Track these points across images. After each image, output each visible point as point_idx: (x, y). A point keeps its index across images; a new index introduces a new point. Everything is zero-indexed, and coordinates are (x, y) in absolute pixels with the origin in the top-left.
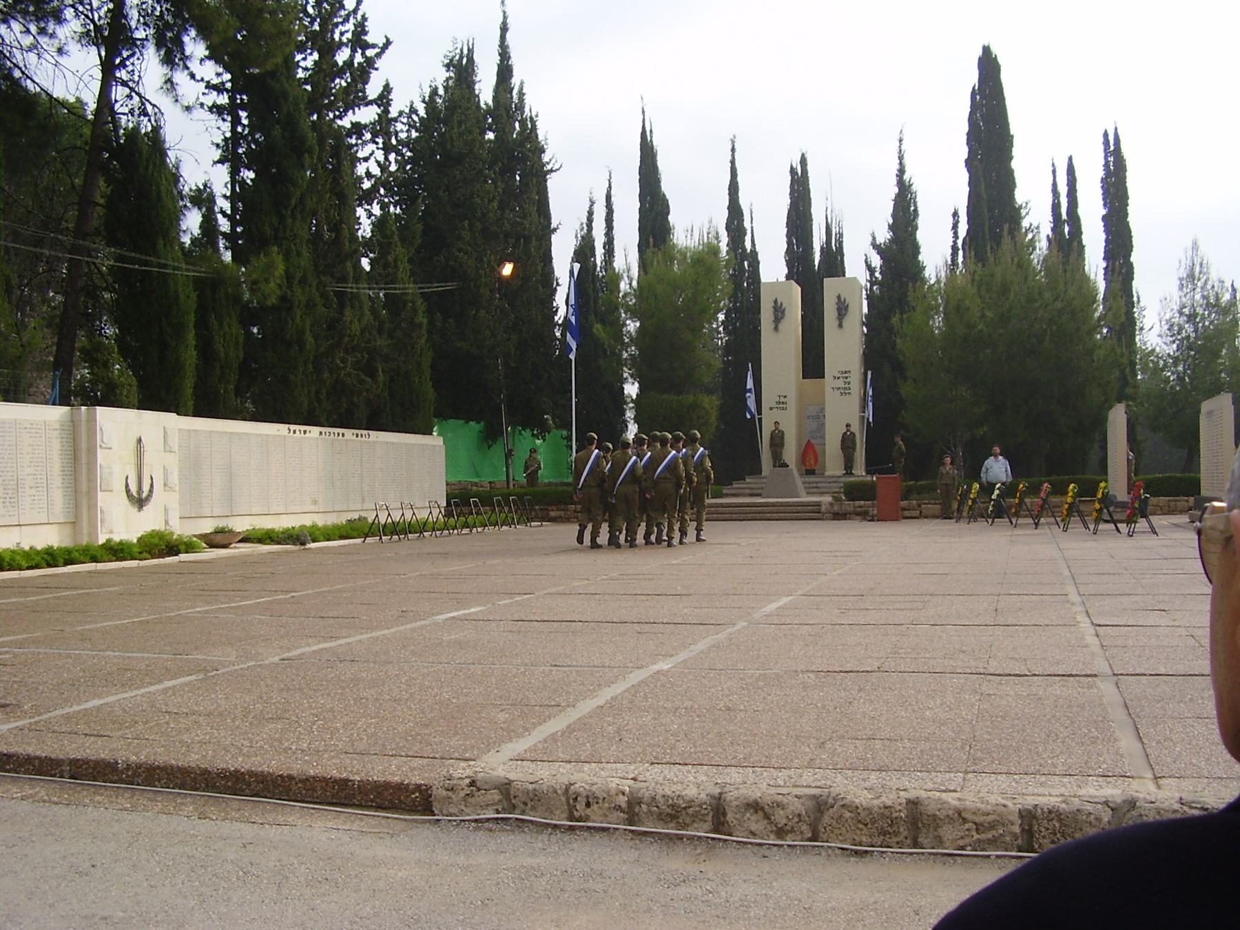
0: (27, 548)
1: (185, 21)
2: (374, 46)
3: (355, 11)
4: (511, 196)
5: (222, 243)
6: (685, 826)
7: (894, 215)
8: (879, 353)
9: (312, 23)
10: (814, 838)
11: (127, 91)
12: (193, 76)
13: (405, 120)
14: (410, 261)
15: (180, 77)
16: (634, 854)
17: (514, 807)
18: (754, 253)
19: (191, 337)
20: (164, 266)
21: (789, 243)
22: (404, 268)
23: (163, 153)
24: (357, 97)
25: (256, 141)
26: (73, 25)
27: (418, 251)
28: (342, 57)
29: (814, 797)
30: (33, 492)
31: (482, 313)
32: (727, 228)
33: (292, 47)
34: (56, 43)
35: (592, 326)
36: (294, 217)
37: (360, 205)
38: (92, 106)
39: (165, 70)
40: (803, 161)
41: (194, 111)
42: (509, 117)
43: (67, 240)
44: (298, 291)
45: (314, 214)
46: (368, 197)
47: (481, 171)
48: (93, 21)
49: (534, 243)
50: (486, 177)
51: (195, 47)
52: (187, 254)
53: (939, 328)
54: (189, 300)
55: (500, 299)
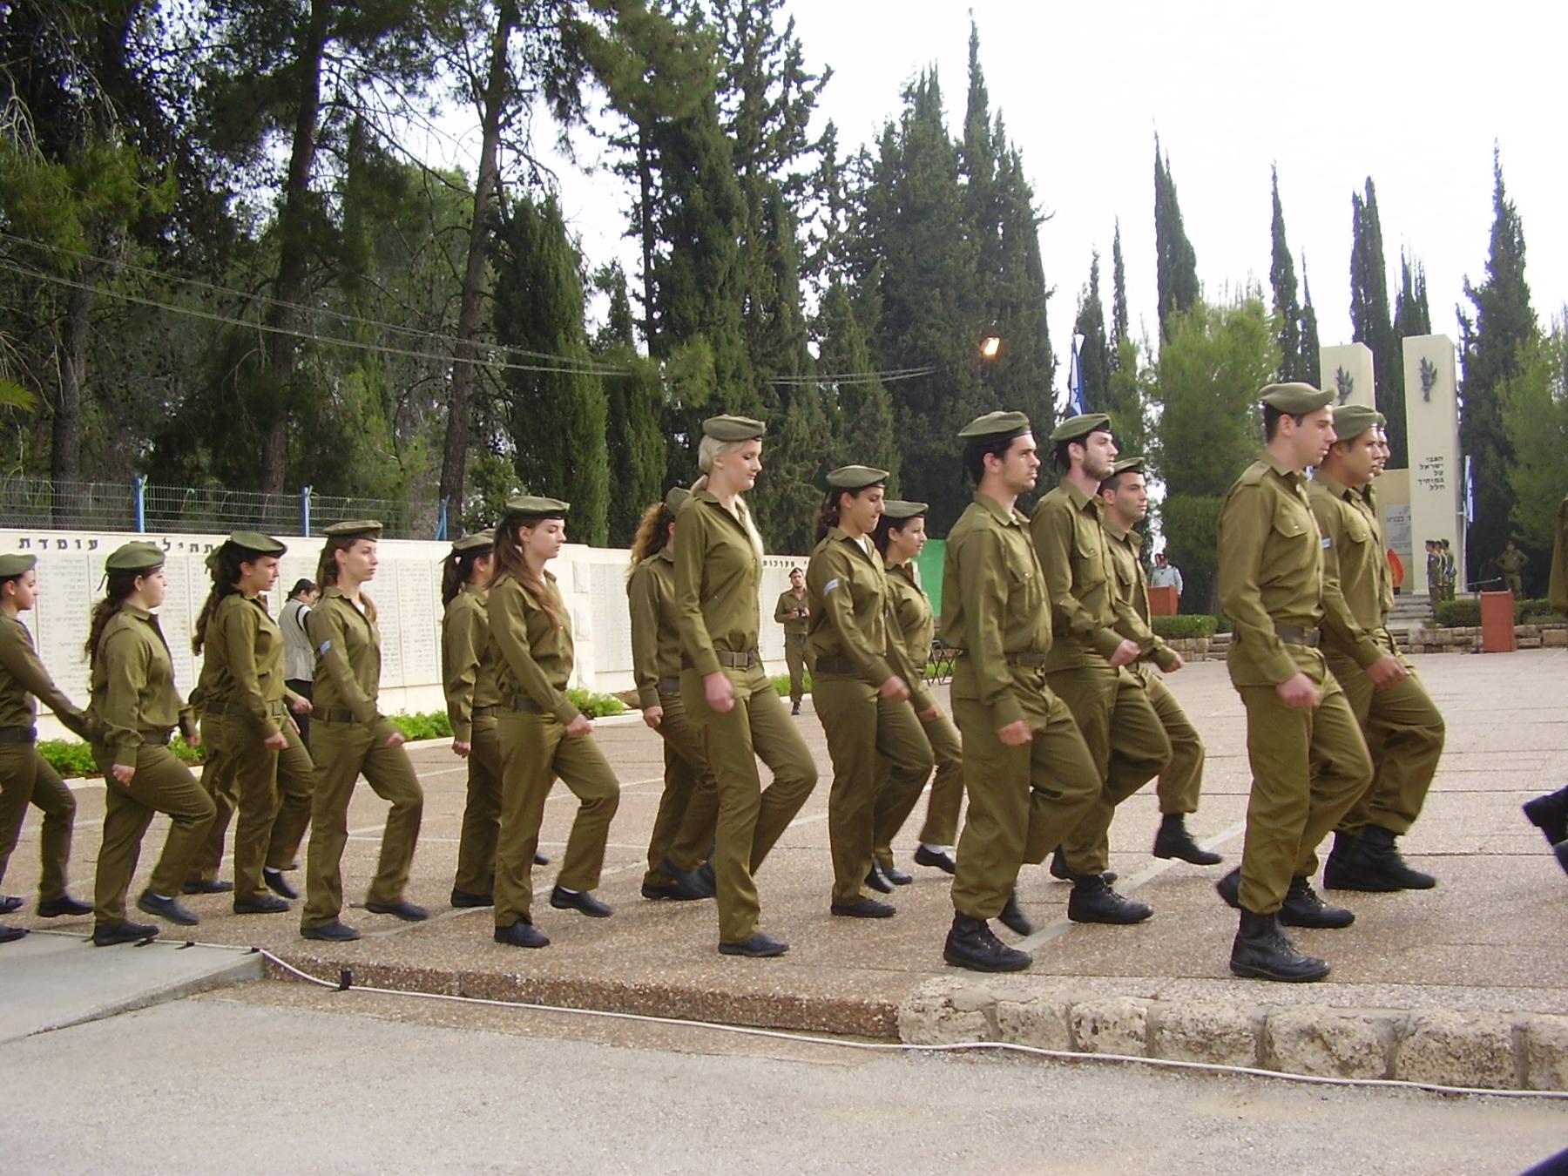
0: (413, 715)
1: (580, 64)
2: (811, 78)
3: (787, 36)
4: (991, 257)
5: (636, 333)
6: (1220, 1058)
7: (1493, 249)
8: (1480, 435)
9: (734, 55)
10: (1390, 1075)
11: (514, 154)
12: (592, 131)
13: (855, 168)
14: (869, 342)
15: (577, 132)
16: (1154, 1094)
17: (1001, 1033)
18: (1309, 310)
19: (603, 446)
20: (567, 365)
21: (1356, 294)
22: (861, 352)
23: (560, 228)
24: (795, 143)
25: (672, 206)
26: (447, 78)
28: (772, 94)
29: (1389, 1022)
30: (419, 646)
31: (962, 404)
32: (1273, 279)
33: (712, 86)
34: (427, 103)
36: (723, 298)
37: (804, 276)
38: (473, 177)
39: (559, 125)
40: (1370, 186)
41: (595, 173)
42: (985, 153)
43: (450, 340)
44: (731, 387)
45: (748, 291)
46: (813, 266)
47: (953, 225)
48: (470, 73)
49: (1024, 312)
50: (961, 232)
51: (593, 94)
52: (594, 349)
53: (1560, 396)
54: (597, 405)
55: (984, 385)
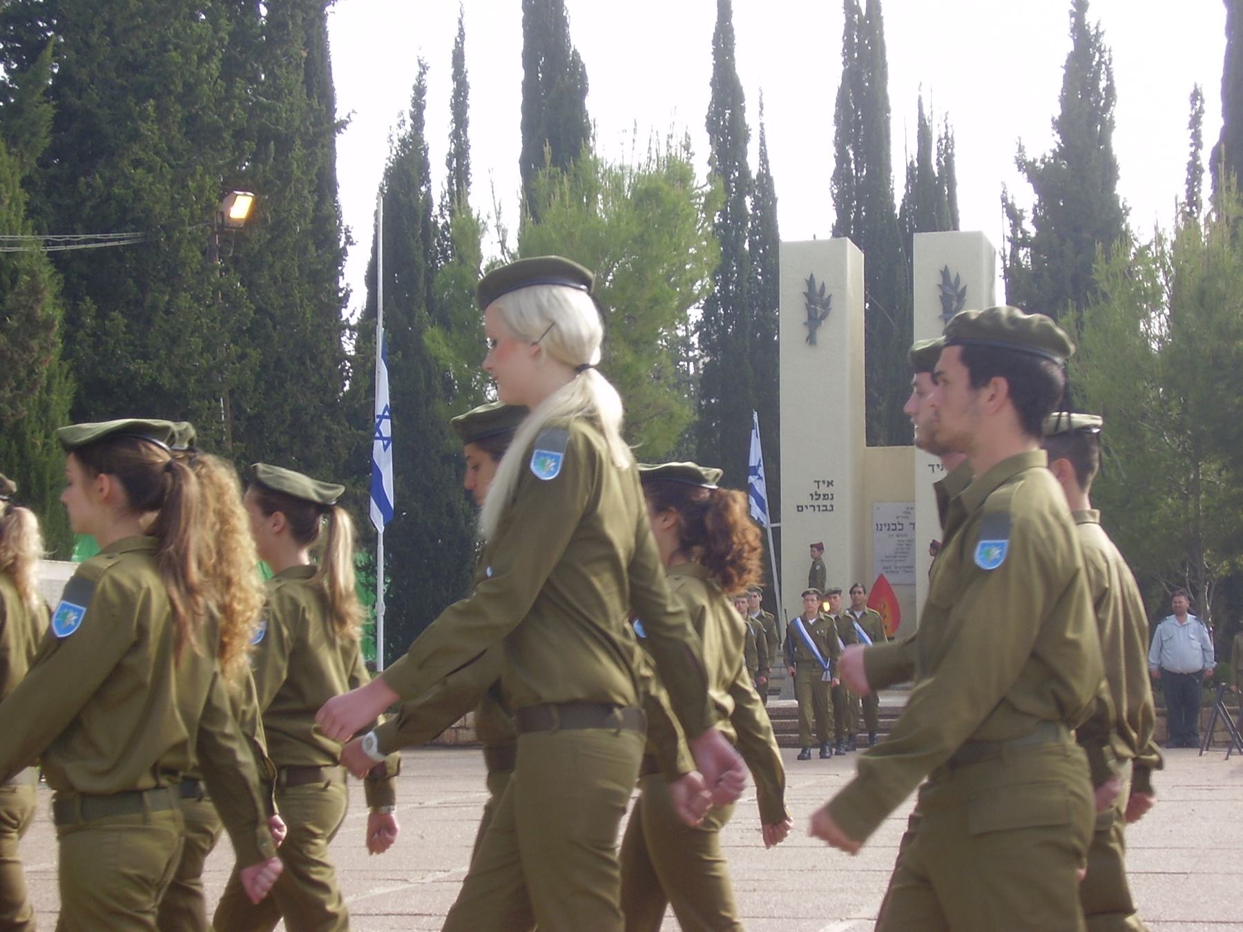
14: (26, 183)
18: (765, 181)
21: (841, 158)
27: (43, 163)
31: (184, 300)
35: (420, 332)
49: (298, 151)
